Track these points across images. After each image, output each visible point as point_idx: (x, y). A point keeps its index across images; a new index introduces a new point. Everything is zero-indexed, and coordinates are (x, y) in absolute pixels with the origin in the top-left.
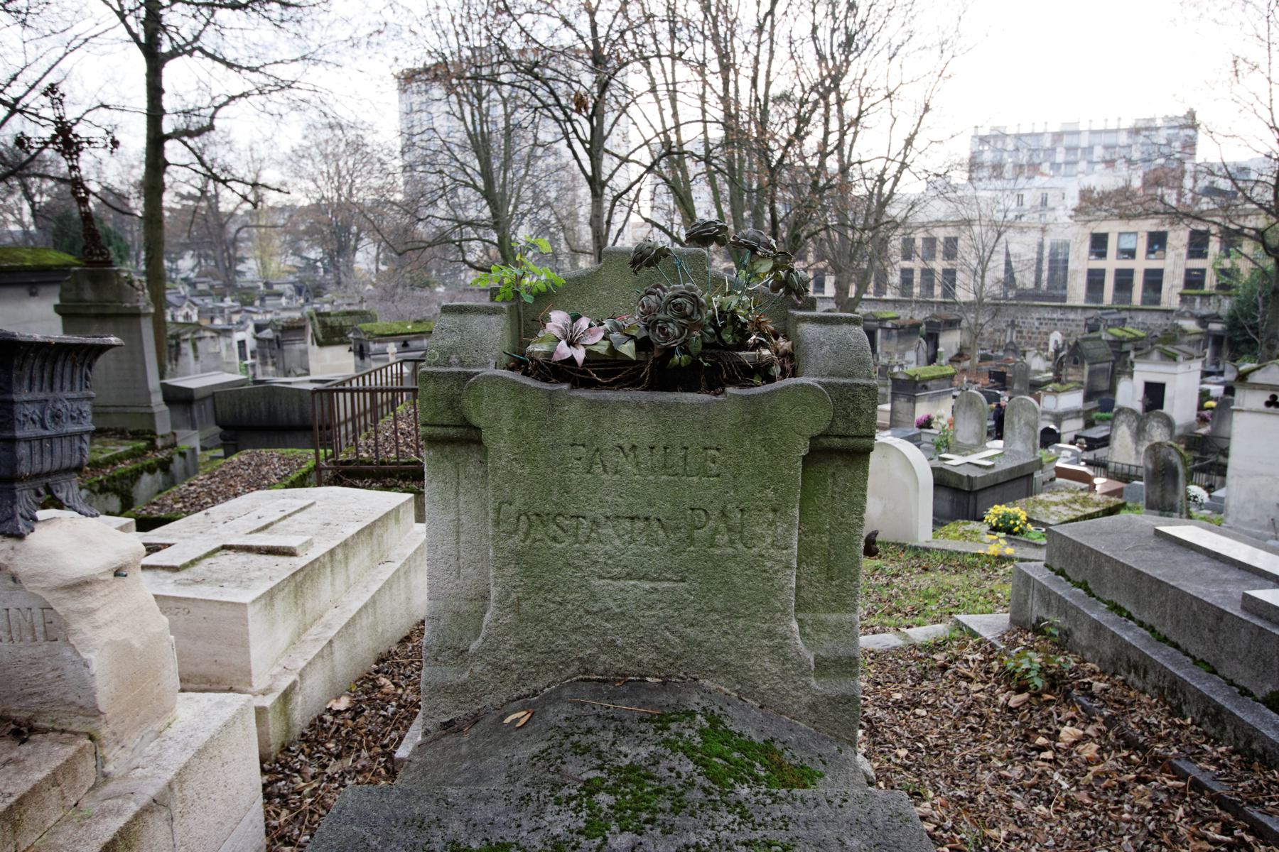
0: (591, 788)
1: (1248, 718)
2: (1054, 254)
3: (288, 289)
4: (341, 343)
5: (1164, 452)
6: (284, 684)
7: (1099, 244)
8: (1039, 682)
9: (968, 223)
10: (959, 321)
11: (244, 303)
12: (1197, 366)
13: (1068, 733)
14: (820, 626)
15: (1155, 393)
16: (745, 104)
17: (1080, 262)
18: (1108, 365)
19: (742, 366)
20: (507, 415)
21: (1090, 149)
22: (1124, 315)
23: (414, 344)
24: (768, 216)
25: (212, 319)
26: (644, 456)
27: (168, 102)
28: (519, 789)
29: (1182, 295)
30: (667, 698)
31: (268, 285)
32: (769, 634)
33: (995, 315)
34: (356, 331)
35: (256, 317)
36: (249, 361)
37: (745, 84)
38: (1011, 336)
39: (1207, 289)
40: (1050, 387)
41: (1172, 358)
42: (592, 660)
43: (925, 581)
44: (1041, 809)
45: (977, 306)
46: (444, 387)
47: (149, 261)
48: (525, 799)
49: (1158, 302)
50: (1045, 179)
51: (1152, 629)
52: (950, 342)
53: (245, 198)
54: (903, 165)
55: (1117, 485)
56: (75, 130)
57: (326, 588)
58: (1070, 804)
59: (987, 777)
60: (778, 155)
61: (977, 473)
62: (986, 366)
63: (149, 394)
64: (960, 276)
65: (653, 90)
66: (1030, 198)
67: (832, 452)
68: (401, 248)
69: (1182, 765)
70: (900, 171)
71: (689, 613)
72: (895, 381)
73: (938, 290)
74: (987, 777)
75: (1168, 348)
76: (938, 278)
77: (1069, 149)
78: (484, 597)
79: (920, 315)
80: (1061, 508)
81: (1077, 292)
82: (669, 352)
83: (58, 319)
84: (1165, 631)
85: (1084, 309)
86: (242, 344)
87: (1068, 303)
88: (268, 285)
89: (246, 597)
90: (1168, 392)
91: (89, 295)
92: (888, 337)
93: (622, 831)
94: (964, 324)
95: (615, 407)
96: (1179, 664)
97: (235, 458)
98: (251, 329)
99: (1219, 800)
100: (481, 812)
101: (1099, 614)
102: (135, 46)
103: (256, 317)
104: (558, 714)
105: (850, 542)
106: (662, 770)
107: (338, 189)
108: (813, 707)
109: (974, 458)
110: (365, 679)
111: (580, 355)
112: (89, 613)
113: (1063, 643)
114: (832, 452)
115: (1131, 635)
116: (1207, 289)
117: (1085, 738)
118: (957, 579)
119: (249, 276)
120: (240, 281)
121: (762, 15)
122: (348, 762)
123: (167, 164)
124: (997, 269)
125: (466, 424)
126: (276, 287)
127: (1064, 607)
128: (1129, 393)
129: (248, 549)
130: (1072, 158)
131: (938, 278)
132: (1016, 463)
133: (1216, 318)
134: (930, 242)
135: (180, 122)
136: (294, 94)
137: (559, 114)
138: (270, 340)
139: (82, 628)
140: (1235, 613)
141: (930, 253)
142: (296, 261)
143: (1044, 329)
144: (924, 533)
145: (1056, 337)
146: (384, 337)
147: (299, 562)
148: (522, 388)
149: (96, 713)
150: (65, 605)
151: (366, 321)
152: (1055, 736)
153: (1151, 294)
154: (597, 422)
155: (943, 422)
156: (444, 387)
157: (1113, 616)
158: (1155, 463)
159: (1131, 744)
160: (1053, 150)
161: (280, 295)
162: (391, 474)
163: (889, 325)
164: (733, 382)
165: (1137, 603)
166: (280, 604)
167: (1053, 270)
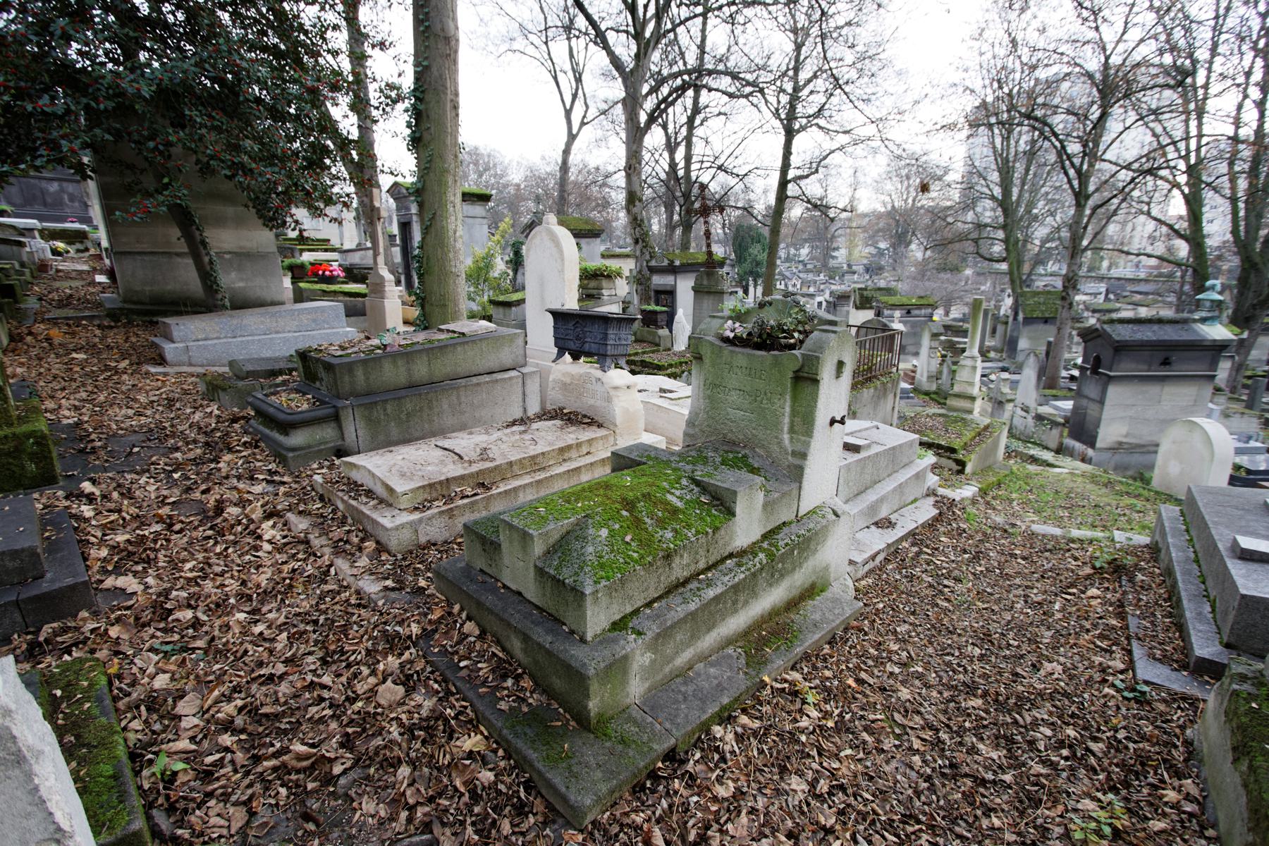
3: (860, 269)
14: (798, 441)
31: (849, 266)
47: (770, 254)
56: (702, 220)
91: (705, 282)
93: (857, 590)
103: (833, 287)
107: (906, 201)
119: (840, 260)
120: (832, 263)
139: (615, 401)
140: (1220, 546)
142: (872, 250)
146: (894, 307)
150: (612, 393)
151: (890, 295)
161: (854, 273)
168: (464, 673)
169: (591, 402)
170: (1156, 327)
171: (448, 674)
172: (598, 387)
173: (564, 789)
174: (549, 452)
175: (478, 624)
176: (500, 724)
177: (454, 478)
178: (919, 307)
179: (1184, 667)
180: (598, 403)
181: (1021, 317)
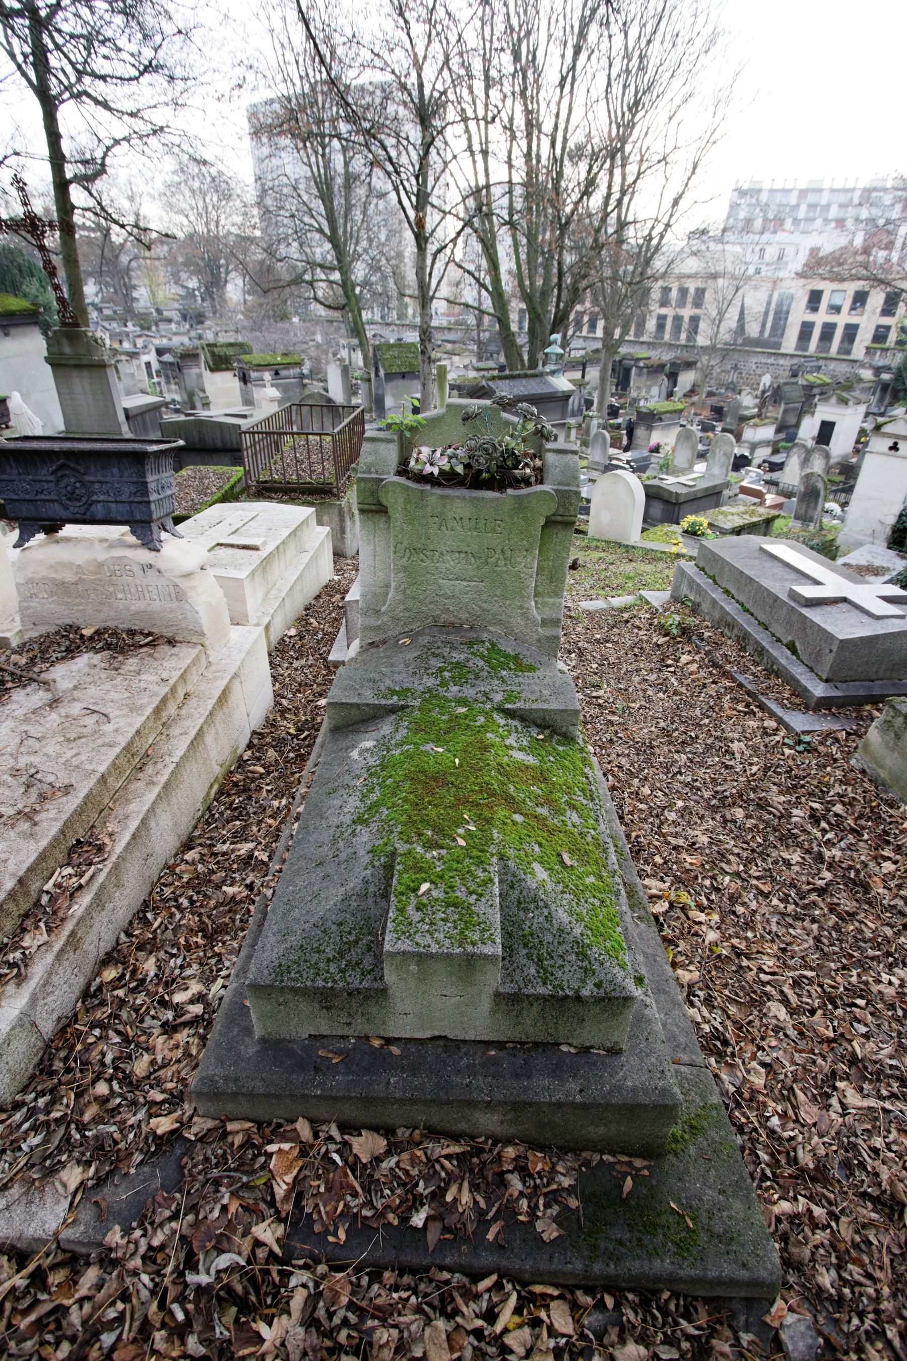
0: (441, 670)
1: (774, 653)
2: (780, 305)
4: (227, 369)
5: (814, 479)
6: (265, 621)
7: (815, 298)
8: (675, 631)
9: (714, 276)
10: (695, 363)
11: (143, 328)
12: (862, 409)
13: (685, 658)
14: (545, 604)
15: (826, 431)
16: (544, 162)
17: (798, 314)
18: (799, 405)
19: (515, 478)
20: (401, 501)
21: (828, 206)
22: (821, 362)
23: (283, 373)
24: (555, 271)
25: (121, 342)
26: (466, 523)
27: (66, 146)
28: (411, 670)
29: (867, 348)
30: (473, 635)
31: (159, 311)
32: (521, 607)
33: (724, 357)
34: (239, 361)
35: (157, 342)
36: (156, 380)
37: (546, 143)
38: (732, 377)
39: (887, 345)
40: (752, 422)
41: (844, 402)
42: (438, 616)
43: (628, 568)
44: (661, 695)
45: (711, 350)
46: (369, 485)
48: (414, 673)
49: (848, 352)
50: (785, 234)
51: (742, 605)
52: (686, 379)
53: (130, 234)
54: (668, 225)
55: (781, 499)
57: (277, 568)
58: (676, 693)
59: (637, 679)
60: (568, 210)
61: (682, 490)
62: (697, 419)
63: (119, 425)
64: (702, 325)
65: (470, 148)
66: (771, 253)
67: (556, 523)
68: (266, 286)
69: (737, 676)
70: (665, 230)
71: (484, 597)
72: (639, 413)
73: (683, 336)
74: (637, 679)
75: (844, 394)
76: (685, 325)
77: (812, 206)
78: (388, 586)
79: (667, 356)
80: (736, 518)
81: (790, 342)
82: (480, 472)
83: (49, 367)
84: (748, 606)
85: (792, 356)
86: (148, 365)
87: (782, 351)
88: (159, 311)
89: (242, 575)
90: (837, 429)
91: (67, 350)
92: (639, 375)
94: (699, 365)
95: (452, 499)
96: (750, 624)
97: (183, 472)
98: (154, 353)
99: (748, 693)
100: (397, 677)
101: (717, 595)
102: (30, 91)
104: (424, 640)
105: (562, 565)
106: (471, 664)
108: (539, 640)
109: (683, 479)
110: (300, 619)
111: (436, 471)
112: (194, 588)
113: (695, 610)
114: (556, 523)
115: (731, 608)
116: (887, 345)
117: (694, 661)
118: (649, 568)
121: (564, 72)
122: (303, 662)
123: (74, 207)
124: (731, 320)
125: (380, 504)
126: (165, 314)
127: (699, 590)
128: (809, 429)
129: (232, 546)
130: (811, 215)
131: (685, 325)
132: (711, 484)
133: (887, 369)
134: (683, 291)
135: (81, 169)
136: (167, 138)
137: (390, 168)
138: (171, 364)
139: (192, 596)
141: (682, 303)
143: (759, 372)
144: (634, 537)
145: (766, 380)
146: (260, 367)
147: (263, 553)
148: (408, 488)
149: (203, 634)
150: (184, 584)
152: (677, 660)
153: (846, 345)
154: (444, 506)
155: (668, 448)
156: (369, 485)
157: (724, 596)
158: (806, 488)
159: (715, 665)
160: (798, 205)
161: (170, 321)
162: (294, 490)
163: (641, 364)
164: (511, 486)
165: (738, 590)
166: (257, 578)
167: (778, 313)
168: (433, 1236)
169: (140, 605)
170: (524, 381)
171: (411, 1258)
172: (151, 578)
173: (744, 1274)
174: (143, 726)
175: (375, 1129)
176: (578, 1265)
177: (31, 870)
178: (288, 366)
179: (807, 708)
180: (156, 606)
181: (382, 373)
